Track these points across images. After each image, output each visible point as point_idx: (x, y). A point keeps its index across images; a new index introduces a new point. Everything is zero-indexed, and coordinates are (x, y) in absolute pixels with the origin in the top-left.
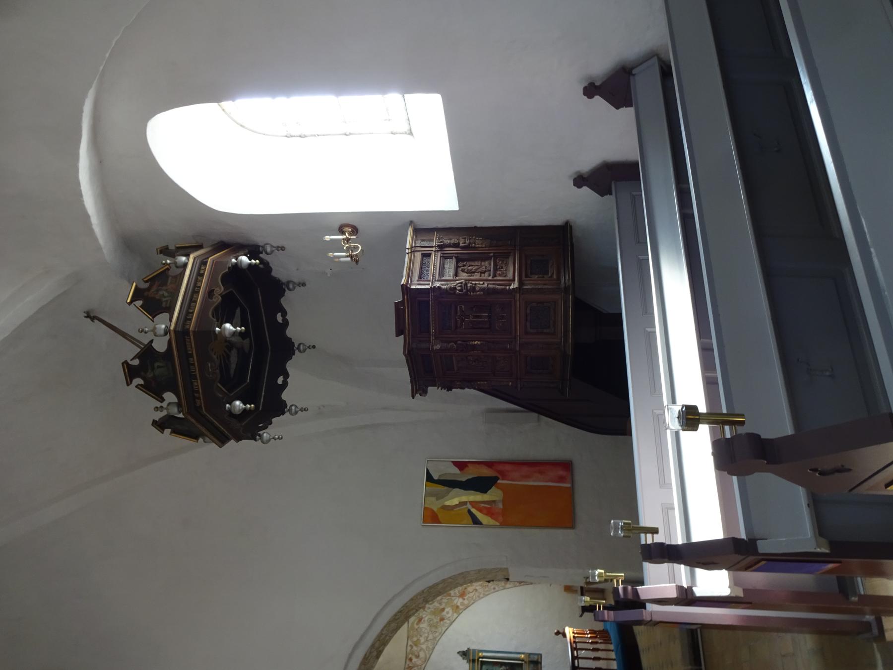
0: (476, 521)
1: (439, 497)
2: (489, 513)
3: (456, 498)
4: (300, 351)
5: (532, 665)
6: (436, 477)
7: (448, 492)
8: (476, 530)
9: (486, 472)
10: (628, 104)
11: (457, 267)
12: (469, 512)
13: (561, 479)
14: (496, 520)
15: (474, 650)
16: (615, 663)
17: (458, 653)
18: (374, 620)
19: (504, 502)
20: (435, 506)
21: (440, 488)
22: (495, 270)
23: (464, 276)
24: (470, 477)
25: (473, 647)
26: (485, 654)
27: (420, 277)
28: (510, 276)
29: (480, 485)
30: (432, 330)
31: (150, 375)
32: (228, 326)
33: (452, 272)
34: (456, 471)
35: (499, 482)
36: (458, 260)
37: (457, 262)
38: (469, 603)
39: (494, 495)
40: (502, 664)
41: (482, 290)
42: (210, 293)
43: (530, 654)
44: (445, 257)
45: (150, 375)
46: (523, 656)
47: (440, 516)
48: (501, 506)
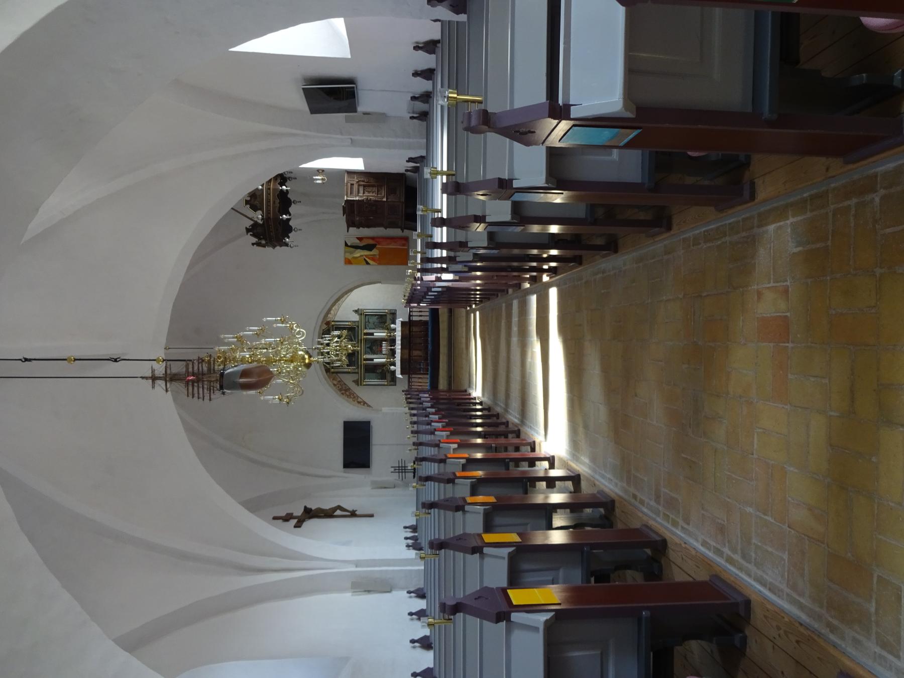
0: (368, 263)
1: (351, 253)
2: (373, 260)
3: (358, 253)
4: (294, 203)
5: (391, 315)
6: (349, 244)
7: (355, 251)
8: (368, 266)
9: (371, 242)
10: (431, 79)
11: (364, 190)
12: (365, 259)
13: (404, 245)
14: (376, 262)
15: (361, 309)
16: (428, 317)
17: (353, 311)
18: (327, 303)
19: (379, 255)
20: (349, 256)
21: (352, 249)
22: (378, 191)
23: (366, 194)
24: (365, 244)
25: (360, 308)
26: (367, 311)
27: (351, 194)
28: (383, 194)
29: (369, 247)
30: (355, 213)
31: (255, 231)
32: (284, 216)
33: (362, 192)
34: (358, 241)
35: (377, 246)
36: (364, 186)
37: (364, 187)
38: (510, 461)
39: (375, 252)
40: (376, 315)
41: (374, 201)
42: (274, 202)
43: (390, 310)
44: (359, 185)
45: (255, 231)
46: (387, 311)
47: (352, 261)
48: (378, 257)
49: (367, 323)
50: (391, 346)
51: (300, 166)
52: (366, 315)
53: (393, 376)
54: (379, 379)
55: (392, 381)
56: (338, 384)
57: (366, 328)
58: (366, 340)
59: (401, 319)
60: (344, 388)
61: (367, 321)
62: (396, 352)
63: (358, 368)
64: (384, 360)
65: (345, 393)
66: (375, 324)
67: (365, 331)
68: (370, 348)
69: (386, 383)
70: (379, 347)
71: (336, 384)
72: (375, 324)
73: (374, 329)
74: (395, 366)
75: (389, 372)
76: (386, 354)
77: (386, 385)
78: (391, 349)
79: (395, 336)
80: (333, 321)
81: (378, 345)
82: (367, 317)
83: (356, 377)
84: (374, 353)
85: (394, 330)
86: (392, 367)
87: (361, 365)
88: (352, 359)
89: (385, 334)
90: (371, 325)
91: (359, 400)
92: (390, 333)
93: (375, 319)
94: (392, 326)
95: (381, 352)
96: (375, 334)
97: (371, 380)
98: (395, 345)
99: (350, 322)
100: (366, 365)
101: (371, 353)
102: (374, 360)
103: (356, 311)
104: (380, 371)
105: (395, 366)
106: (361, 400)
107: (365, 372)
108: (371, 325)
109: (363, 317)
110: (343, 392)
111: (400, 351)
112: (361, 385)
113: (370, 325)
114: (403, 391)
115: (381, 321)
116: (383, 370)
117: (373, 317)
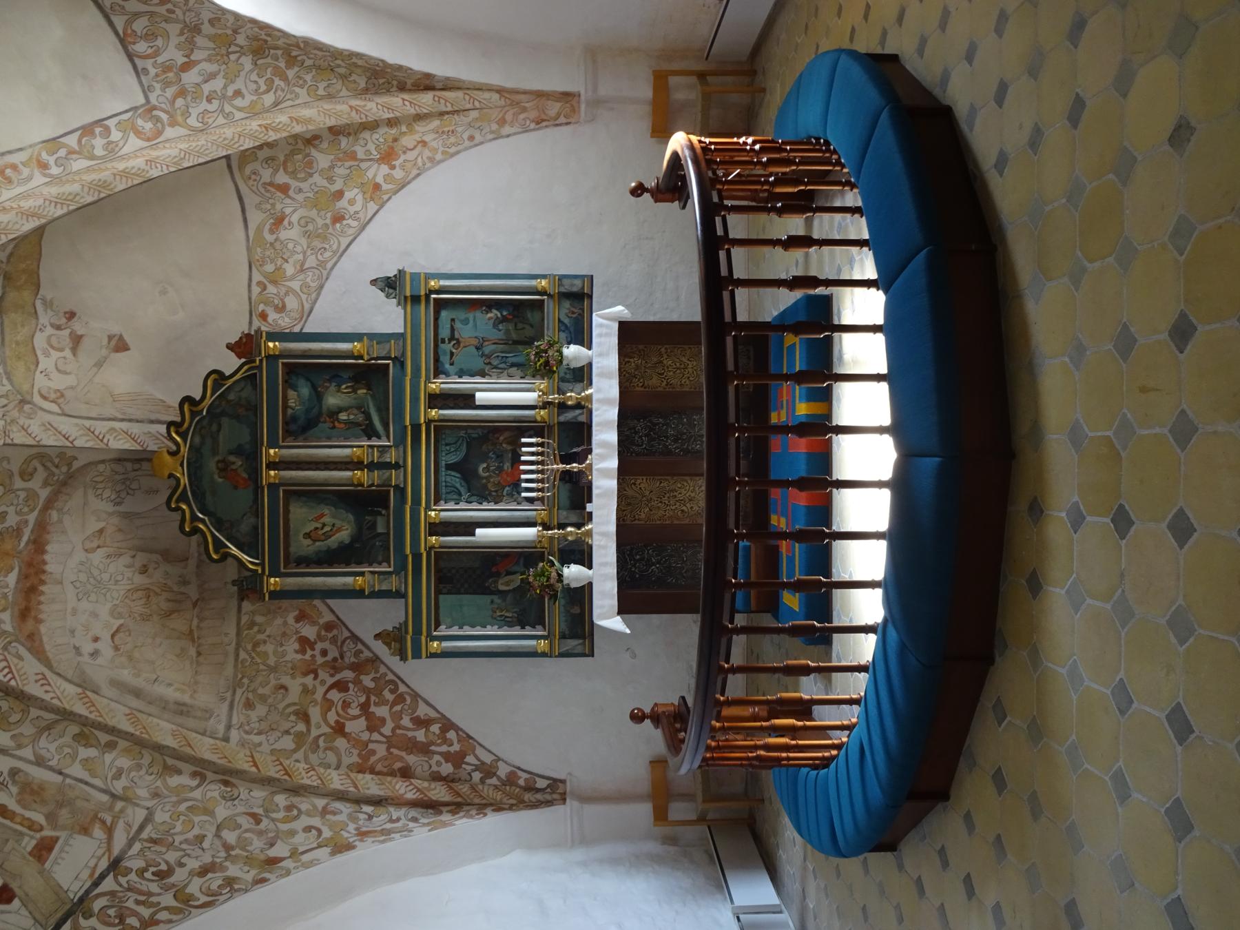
5: (567, 304)
15: (415, 277)
17: (374, 282)
26: (443, 283)
46: (544, 283)
49: (447, 347)
50: (566, 459)
51: (628, 631)
52: (440, 305)
53: (576, 610)
54: (510, 625)
56: (320, 638)
57: (438, 371)
58: (441, 429)
59: (620, 310)
60: (350, 658)
61: (445, 332)
62: (595, 492)
63: (401, 568)
64: (530, 533)
65: (357, 682)
66: (488, 349)
67: (437, 385)
68: (464, 469)
69: (543, 645)
70: (507, 466)
71: (312, 637)
72: (488, 349)
73: (483, 375)
75: (554, 597)
76: (541, 499)
77: (544, 655)
78: (567, 476)
79: (583, 406)
80: (272, 336)
81: (500, 457)
83: (391, 614)
84: (482, 494)
85: (582, 375)
86: (573, 572)
87: (417, 557)
88: (373, 526)
89: (530, 397)
90: (467, 356)
91: (422, 711)
92: (560, 391)
93: (479, 326)
96: (479, 395)
98: (590, 451)
100: (441, 557)
102: (479, 531)
103: (390, 285)
105: (590, 567)
106: (433, 714)
107: (438, 592)
108: (467, 356)
109: (425, 313)
111: (613, 484)
112: (417, 655)
115: (514, 336)
116: (525, 586)
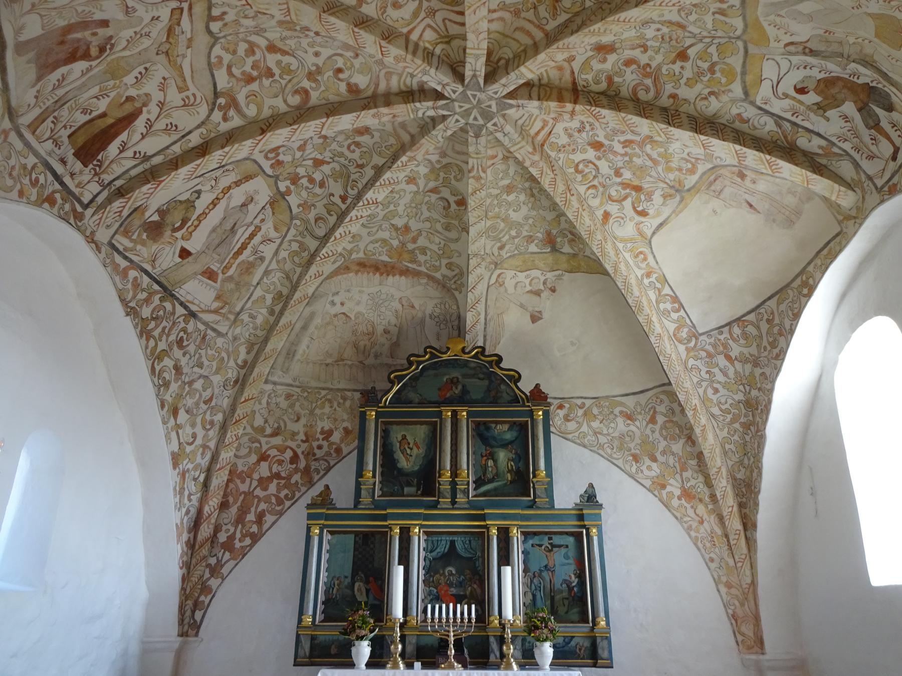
5: (587, 644)
15: (598, 517)
17: (591, 486)
26: (595, 539)
40: (581, 576)
43: (608, 639)
50: (458, 644)
52: (578, 537)
54: (326, 592)
55: (312, 648)
58: (482, 536)
60: (314, 465)
61: (557, 540)
63: (377, 505)
65: (296, 470)
68: (451, 555)
69: (308, 620)
70: (453, 591)
71: (332, 439)
73: (526, 571)
74: (369, 665)
77: (300, 621)
78: (443, 644)
80: (546, 414)
81: (460, 584)
82: (571, 540)
84: (431, 569)
86: (364, 650)
87: (384, 518)
88: (409, 484)
89: (508, 613)
90: (540, 558)
91: (269, 519)
93: (565, 571)
94: (547, 651)
95: (437, 599)
96: (508, 569)
97: (325, 557)
99: (549, 474)
100: (384, 536)
101: (430, 556)
103: (590, 497)
104: (361, 598)
105: (369, 665)
106: (265, 527)
107: (357, 534)
108: (540, 558)
109: (571, 524)
110: (302, 464)
112: (310, 517)
113: (539, 553)
114: (840, 116)
117: (573, 567)
